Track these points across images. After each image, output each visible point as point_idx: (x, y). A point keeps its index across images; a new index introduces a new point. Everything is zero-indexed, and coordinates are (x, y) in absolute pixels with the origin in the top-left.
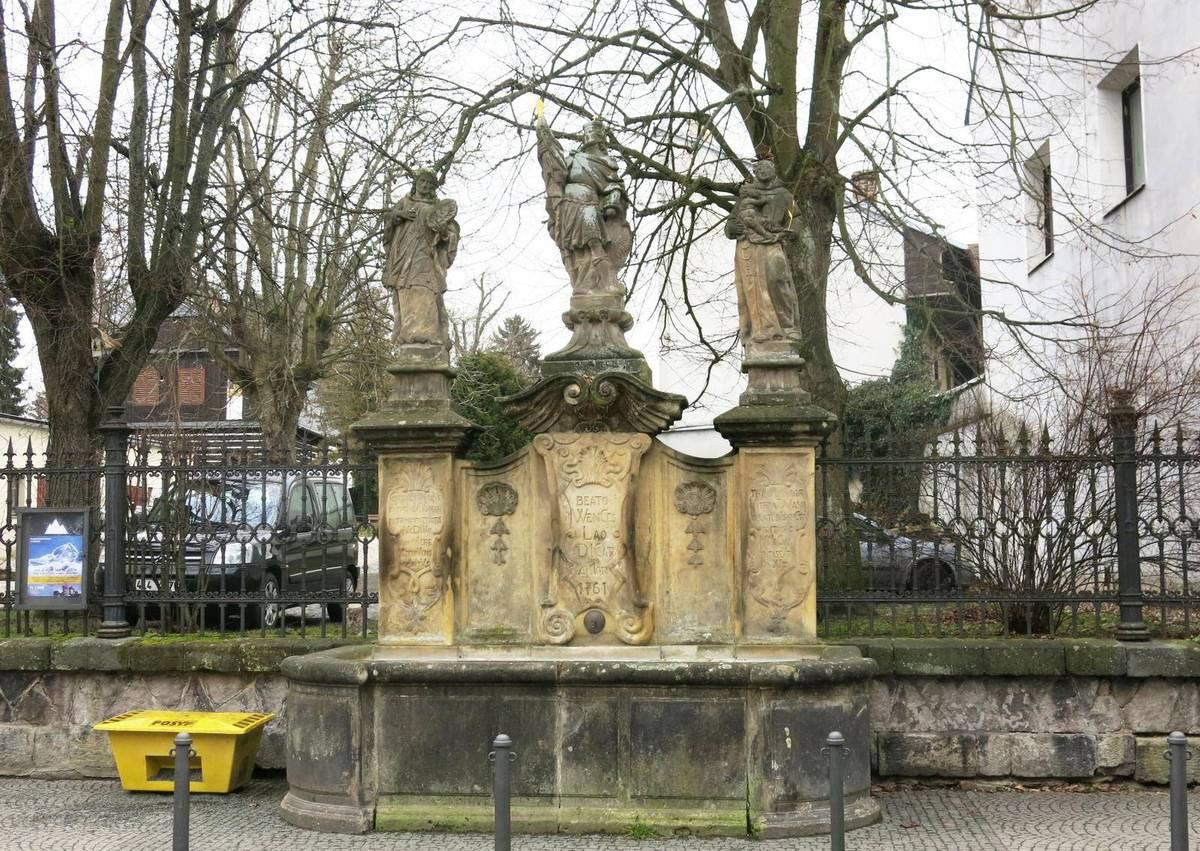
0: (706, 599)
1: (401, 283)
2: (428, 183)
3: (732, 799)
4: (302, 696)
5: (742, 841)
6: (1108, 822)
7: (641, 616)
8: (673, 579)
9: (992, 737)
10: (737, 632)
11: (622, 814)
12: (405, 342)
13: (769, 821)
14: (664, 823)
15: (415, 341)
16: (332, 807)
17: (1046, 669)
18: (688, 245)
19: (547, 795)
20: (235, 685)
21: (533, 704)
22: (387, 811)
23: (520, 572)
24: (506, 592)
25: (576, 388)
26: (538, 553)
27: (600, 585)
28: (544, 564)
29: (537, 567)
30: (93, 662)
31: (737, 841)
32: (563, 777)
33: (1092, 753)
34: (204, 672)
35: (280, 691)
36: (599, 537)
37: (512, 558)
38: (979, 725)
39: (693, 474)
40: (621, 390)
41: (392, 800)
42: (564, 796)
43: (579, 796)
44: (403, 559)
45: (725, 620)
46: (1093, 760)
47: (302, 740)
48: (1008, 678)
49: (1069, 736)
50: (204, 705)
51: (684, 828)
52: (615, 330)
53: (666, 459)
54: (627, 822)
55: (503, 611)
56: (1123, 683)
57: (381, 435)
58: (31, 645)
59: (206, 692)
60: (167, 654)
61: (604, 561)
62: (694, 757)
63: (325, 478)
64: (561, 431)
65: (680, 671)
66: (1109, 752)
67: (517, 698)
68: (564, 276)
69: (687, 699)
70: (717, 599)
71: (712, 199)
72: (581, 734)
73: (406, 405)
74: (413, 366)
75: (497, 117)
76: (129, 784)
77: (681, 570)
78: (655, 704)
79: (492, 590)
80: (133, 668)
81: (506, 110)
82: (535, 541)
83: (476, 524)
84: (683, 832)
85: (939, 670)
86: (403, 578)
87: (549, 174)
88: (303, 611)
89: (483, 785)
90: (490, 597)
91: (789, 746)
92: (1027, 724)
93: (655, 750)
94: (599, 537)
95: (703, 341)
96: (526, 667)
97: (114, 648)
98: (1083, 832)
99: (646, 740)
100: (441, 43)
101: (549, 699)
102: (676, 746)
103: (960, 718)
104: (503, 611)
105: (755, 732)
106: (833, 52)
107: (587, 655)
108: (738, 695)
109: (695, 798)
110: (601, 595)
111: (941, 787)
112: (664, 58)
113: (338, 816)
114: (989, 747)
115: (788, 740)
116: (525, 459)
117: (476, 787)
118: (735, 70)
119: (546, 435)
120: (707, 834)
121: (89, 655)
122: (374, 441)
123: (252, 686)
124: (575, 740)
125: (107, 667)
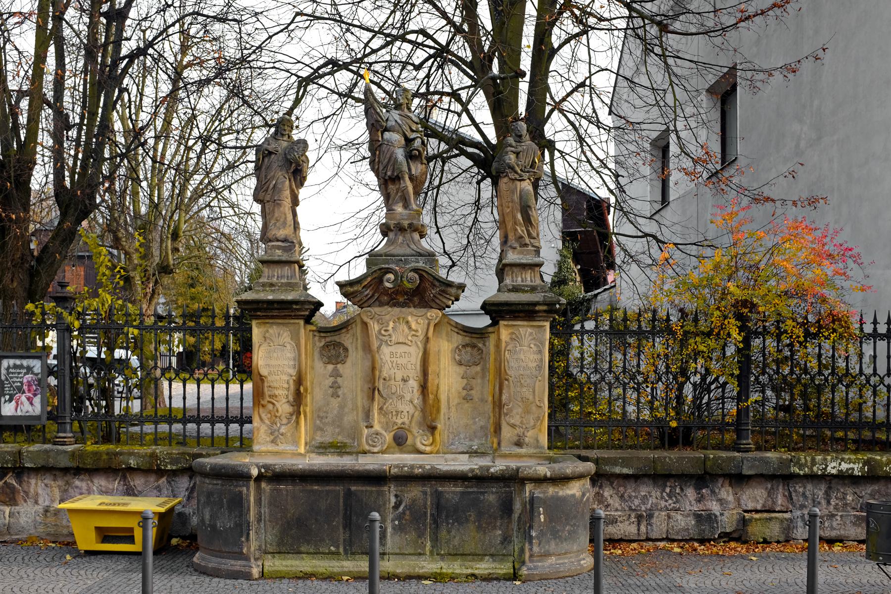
0: (475, 423)
1: (268, 198)
2: (283, 126)
4: (210, 486)
7: (433, 434)
8: (453, 409)
9: (656, 514)
10: (495, 445)
13: (528, 569)
14: (458, 571)
16: (233, 562)
17: (692, 471)
18: (438, 187)
20: (152, 478)
21: (372, 492)
22: (274, 564)
23: (350, 405)
25: (391, 276)
26: (362, 391)
27: (405, 413)
28: (366, 398)
29: (361, 400)
30: (51, 462)
34: (130, 469)
35: (184, 483)
36: (405, 380)
37: (344, 394)
38: (649, 506)
39: (467, 338)
40: (421, 276)
42: (392, 554)
45: (487, 437)
47: (211, 516)
48: (667, 477)
50: (130, 492)
51: (473, 575)
52: (416, 236)
53: (449, 328)
55: (337, 430)
56: (738, 479)
57: (255, 306)
58: (6, 449)
59: (132, 484)
60: (105, 457)
61: (408, 397)
62: (479, 528)
64: (380, 306)
66: (728, 521)
67: (360, 488)
68: (377, 197)
69: (475, 489)
70: (482, 423)
71: (463, 153)
72: (404, 513)
73: (272, 285)
74: (276, 258)
75: (322, 86)
76: (82, 546)
78: (453, 492)
79: (330, 415)
80: (81, 466)
81: (328, 81)
85: (625, 471)
87: (373, 124)
89: (338, 547)
90: (329, 420)
91: (542, 520)
92: (677, 506)
93: (453, 523)
94: (405, 380)
95: (445, 252)
99: (447, 517)
100: (282, 31)
101: (382, 489)
102: (467, 520)
103: (637, 502)
104: (337, 430)
105: (519, 511)
108: (509, 487)
109: (479, 555)
110: (406, 420)
112: (432, 51)
113: (237, 568)
114: (654, 520)
115: (542, 516)
116: (354, 325)
117: (332, 548)
118: (478, 67)
119: (369, 309)
120: (488, 579)
121: (49, 457)
122: (250, 310)
123: (164, 479)
125: (62, 465)
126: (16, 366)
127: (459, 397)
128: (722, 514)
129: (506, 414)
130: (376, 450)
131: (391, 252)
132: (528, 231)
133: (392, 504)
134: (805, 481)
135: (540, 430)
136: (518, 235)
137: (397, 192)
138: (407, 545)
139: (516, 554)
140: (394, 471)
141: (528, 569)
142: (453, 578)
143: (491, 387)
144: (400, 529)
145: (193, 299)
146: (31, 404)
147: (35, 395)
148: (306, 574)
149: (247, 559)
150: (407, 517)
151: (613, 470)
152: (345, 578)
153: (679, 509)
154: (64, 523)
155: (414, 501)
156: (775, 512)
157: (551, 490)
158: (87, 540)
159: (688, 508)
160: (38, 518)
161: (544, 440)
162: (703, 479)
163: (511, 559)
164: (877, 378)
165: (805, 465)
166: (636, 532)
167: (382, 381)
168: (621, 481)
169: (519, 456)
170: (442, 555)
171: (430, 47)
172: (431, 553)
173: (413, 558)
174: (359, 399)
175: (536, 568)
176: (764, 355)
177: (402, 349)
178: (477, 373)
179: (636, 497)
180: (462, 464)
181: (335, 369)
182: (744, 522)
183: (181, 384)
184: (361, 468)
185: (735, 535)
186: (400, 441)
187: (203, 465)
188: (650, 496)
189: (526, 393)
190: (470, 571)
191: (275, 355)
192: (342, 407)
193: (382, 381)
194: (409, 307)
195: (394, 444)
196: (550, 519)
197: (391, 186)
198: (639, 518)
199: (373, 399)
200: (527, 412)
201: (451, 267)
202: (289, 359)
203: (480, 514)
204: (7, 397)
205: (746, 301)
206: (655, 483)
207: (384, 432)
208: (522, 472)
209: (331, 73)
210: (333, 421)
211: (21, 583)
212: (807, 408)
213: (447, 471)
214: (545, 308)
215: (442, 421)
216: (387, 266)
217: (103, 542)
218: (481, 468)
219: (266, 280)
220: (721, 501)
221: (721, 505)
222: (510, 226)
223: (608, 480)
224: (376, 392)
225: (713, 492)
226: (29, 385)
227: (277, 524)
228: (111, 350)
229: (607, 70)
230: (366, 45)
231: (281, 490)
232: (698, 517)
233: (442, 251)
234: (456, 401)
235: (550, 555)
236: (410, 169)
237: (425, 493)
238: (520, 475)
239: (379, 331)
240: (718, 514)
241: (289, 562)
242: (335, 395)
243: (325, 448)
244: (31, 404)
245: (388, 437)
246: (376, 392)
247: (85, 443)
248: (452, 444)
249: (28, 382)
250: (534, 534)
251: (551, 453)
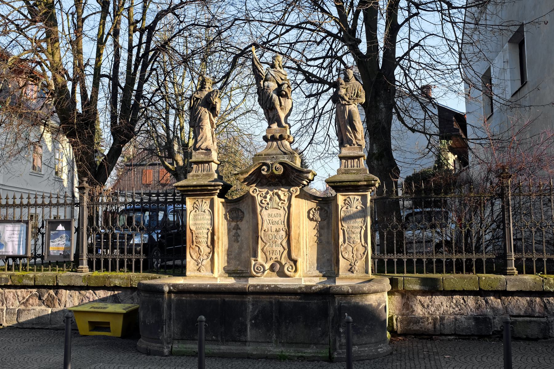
0: (324, 257)
3: (323, 344)
5: (326, 363)
6: (493, 356)
11: (275, 350)
13: (338, 354)
16: (154, 344)
19: (242, 341)
22: (177, 346)
31: (324, 363)
32: (250, 334)
33: (491, 324)
37: (242, 240)
41: (179, 342)
42: (251, 342)
43: (257, 342)
45: (332, 266)
46: (491, 327)
49: (480, 317)
51: (302, 356)
54: (278, 353)
55: (238, 263)
63: (174, 206)
65: (300, 288)
69: (303, 301)
70: (328, 257)
72: (258, 315)
73: (197, 176)
82: (251, 233)
84: (302, 358)
88: (174, 262)
89: (217, 336)
96: (291, 287)
97: (81, 277)
98: (480, 360)
104: (238, 263)
106: (393, 28)
107: (272, 281)
109: (307, 344)
111: (425, 339)
113: (156, 348)
120: (311, 359)
121: (71, 279)
123: (136, 293)
124: (255, 318)
125: (79, 285)
141: (338, 354)
142: (290, 359)
144: (255, 326)
149: (162, 343)
150: (260, 318)
156: (534, 317)
167: (263, 232)
172: (276, 341)
191: (199, 217)
192: (240, 248)
193: (263, 232)
202: (208, 219)
207: (264, 264)
208: (332, 289)
210: (235, 257)
213: (284, 289)
219: (194, 173)
239: (261, 201)
241: (188, 346)
246: (260, 239)
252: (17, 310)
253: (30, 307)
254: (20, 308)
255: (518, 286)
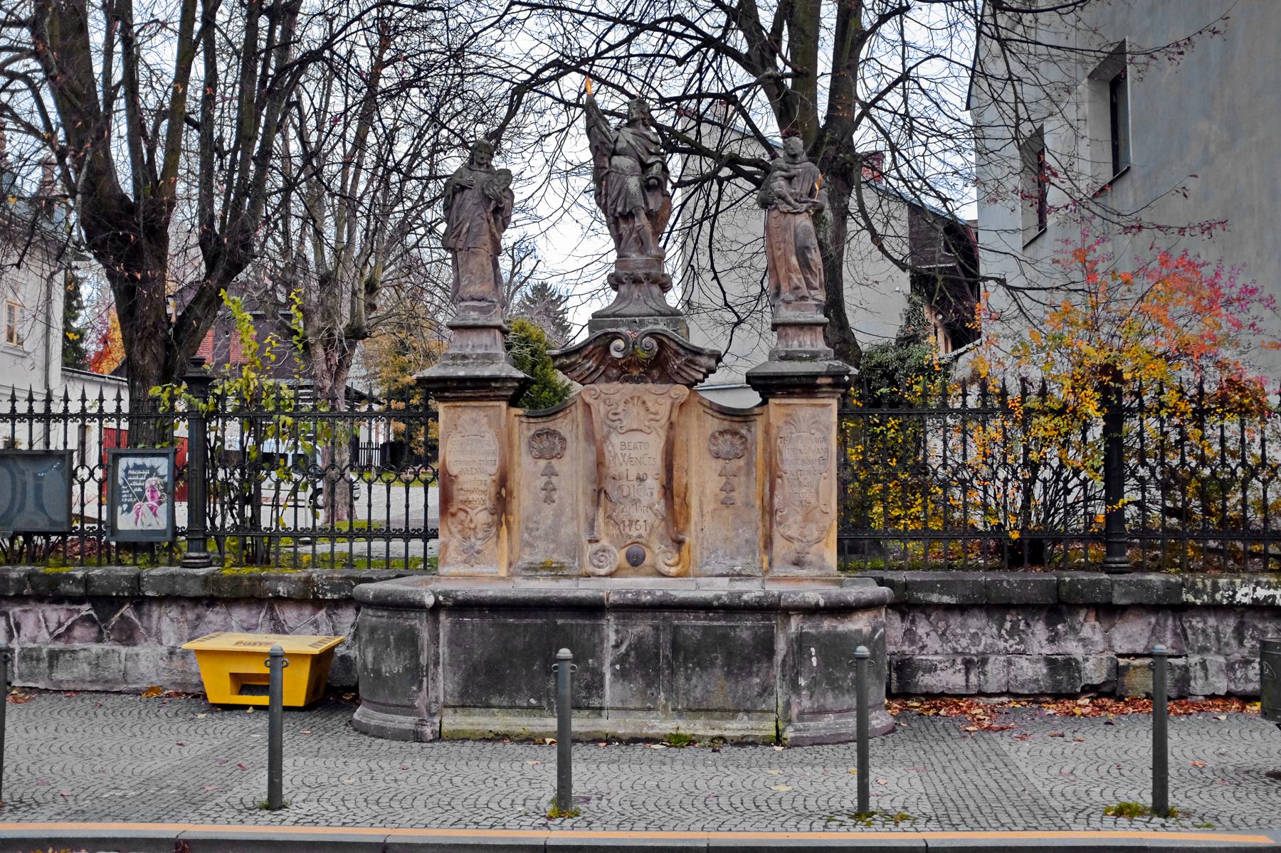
0: (738, 535)
1: (460, 245)
4: (374, 619)
7: (679, 550)
8: (708, 518)
9: (992, 658)
10: (765, 565)
11: (664, 725)
12: (463, 300)
13: (796, 730)
14: (701, 733)
15: (473, 299)
16: (401, 718)
17: (1040, 600)
18: (715, 216)
20: (307, 611)
22: (453, 721)
24: (555, 528)
25: (620, 343)
27: (641, 523)
29: (584, 506)
32: (611, 691)
33: (1080, 672)
34: (279, 599)
35: (348, 617)
37: (561, 499)
39: (726, 423)
40: (661, 343)
43: (625, 709)
44: (461, 498)
51: (721, 738)
52: (656, 290)
53: (701, 409)
55: (552, 546)
56: (1108, 611)
57: (441, 385)
59: (281, 618)
62: (729, 674)
64: (607, 382)
66: (1095, 672)
67: (569, 621)
69: (723, 623)
70: (747, 536)
72: (627, 654)
73: (464, 357)
74: (471, 322)
76: (213, 699)
77: (715, 510)
78: (694, 627)
79: (542, 527)
80: (215, 594)
82: (581, 484)
83: (528, 471)
85: (946, 599)
86: (461, 515)
89: (539, 699)
90: (541, 532)
91: (815, 664)
92: (1022, 647)
93: (693, 669)
94: (641, 479)
95: (726, 304)
99: (686, 659)
100: (492, 25)
102: (713, 664)
103: (964, 642)
104: (552, 546)
105: (784, 652)
106: (851, 39)
108: (769, 620)
110: (642, 532)
112: (695, 43)
114: (988, 668)
115: (814, 659)
116: (573, 408)
117: (532, 701)
118: (757, 61)
122: (435, 391)
123: (323, 612)
124: (622, 659)
125: (191, 594)
126: (136, 467)
127: (716, 501)
128: (1086, 660)
129: (780, 524)
130: (602, 572)
131: (622, 312)
132: (806, 279)
133: (613, 643)
134: (1206, 614)
135: (827, 544)
136: (793, 285)
137: (631, 234)
138: (633, 696)
139: (780, 710)
140: (614, 598)
141: (796, 730)
142: (691, 741)
143: (759, 488)
144: (623, 675)
145: (403, 370)
146: (155, 514)
147: (160, 503)
148: (497, 734)
150: (631, 660)
151: (929, 599)
152: (548, 740)
153: (1024, 653)
154: (194, 669)
155: (640, 638)
157: (827, 624)
158: (221, 691)
159: (1036, 650)
160: (161, 662)
161: (831, 557)
162: (1057, 608)
163: (774, 716)
164: (422, 477)
165: (1203, 591)
166: (964, 683)
168: (941, 613)
169: (799, 579)
170: (679, 711)
171: (692, 37)
173: (641, 714)
174: (581, 504)
175: (806, 729)
176: (1142, 440)
177: (639, 437)
178: (739, 468)
179: (963, 636)
180: (715, 589)
181: (549, 466)
182: (1119, 671)
183: (385, 487)
184: (570, 595)
185: (1106, 689)
186: (635, 561)
187: (363, 593)
188: (978, 632)
189: (806, 494)
190: (716, 733)
191: (468, 448)
192: (558, 515)
194: (646, 382)
195: (627, 565)
196: (826, 661)
197: (623, 225)
198: (968, 664)
199: (598, 505)
200: (807, 519)
201: (736, 325)
203: (730, 656)
204: (125, 506)
205: (1107, 366)
206: (989, 616)
209: (555, 78)
211: (133, 741)
212: (1207, 511)
214: (829, 381)
215: (694, 534)
216: (614, 330)
217: (240, 693)
218: (731, 594)
220: (1085, 642)
221: (1085, 646)
222: (782, 273)
223: (923, 612)
224: (603, 495)
225: (1072, 628)
226: (153, 491)
227: (459, 668)
228: (259, 442)
229: (938, 56)
230: (600, 39)
231: (464, 623)
232: (1050, 662)
233: (721, 303)
234: (711, 508)
235: (827, 712)
236: (647, 203)
237: (656, 628)
238: (782, 604)
240: (1080, 659)
242: (549, 500)
243: (536, 570)
244: (155, 514)
245: (620, 557)
246: (603, 495)
247: (223, 565)
248: (707, 564)
249: (152, 487)
250: (802, 682)
251: (843, 576)
252: (45, 651)
253: (77, 645)
254: (51, 646)
255: (1133, 593)
